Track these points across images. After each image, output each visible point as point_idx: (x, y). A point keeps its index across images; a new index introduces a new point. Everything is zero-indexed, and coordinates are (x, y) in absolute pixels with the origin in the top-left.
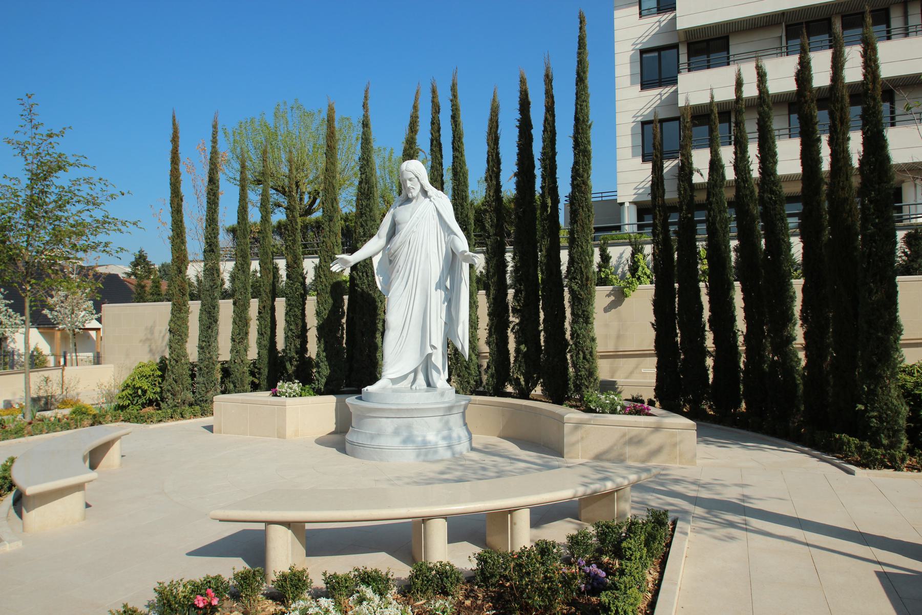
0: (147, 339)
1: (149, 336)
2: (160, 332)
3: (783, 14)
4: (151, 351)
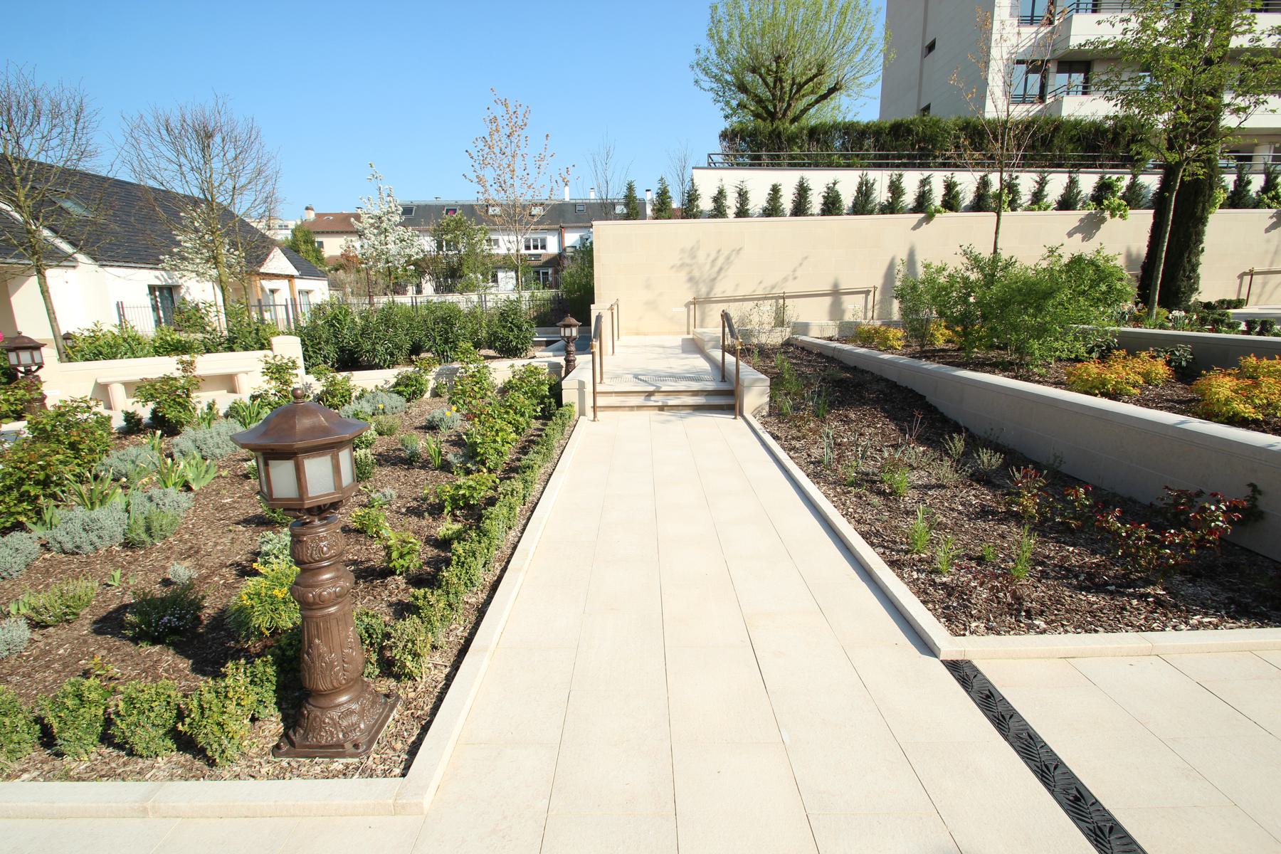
0: (682, 265)
1: (688, 261)
4: (691, 279)
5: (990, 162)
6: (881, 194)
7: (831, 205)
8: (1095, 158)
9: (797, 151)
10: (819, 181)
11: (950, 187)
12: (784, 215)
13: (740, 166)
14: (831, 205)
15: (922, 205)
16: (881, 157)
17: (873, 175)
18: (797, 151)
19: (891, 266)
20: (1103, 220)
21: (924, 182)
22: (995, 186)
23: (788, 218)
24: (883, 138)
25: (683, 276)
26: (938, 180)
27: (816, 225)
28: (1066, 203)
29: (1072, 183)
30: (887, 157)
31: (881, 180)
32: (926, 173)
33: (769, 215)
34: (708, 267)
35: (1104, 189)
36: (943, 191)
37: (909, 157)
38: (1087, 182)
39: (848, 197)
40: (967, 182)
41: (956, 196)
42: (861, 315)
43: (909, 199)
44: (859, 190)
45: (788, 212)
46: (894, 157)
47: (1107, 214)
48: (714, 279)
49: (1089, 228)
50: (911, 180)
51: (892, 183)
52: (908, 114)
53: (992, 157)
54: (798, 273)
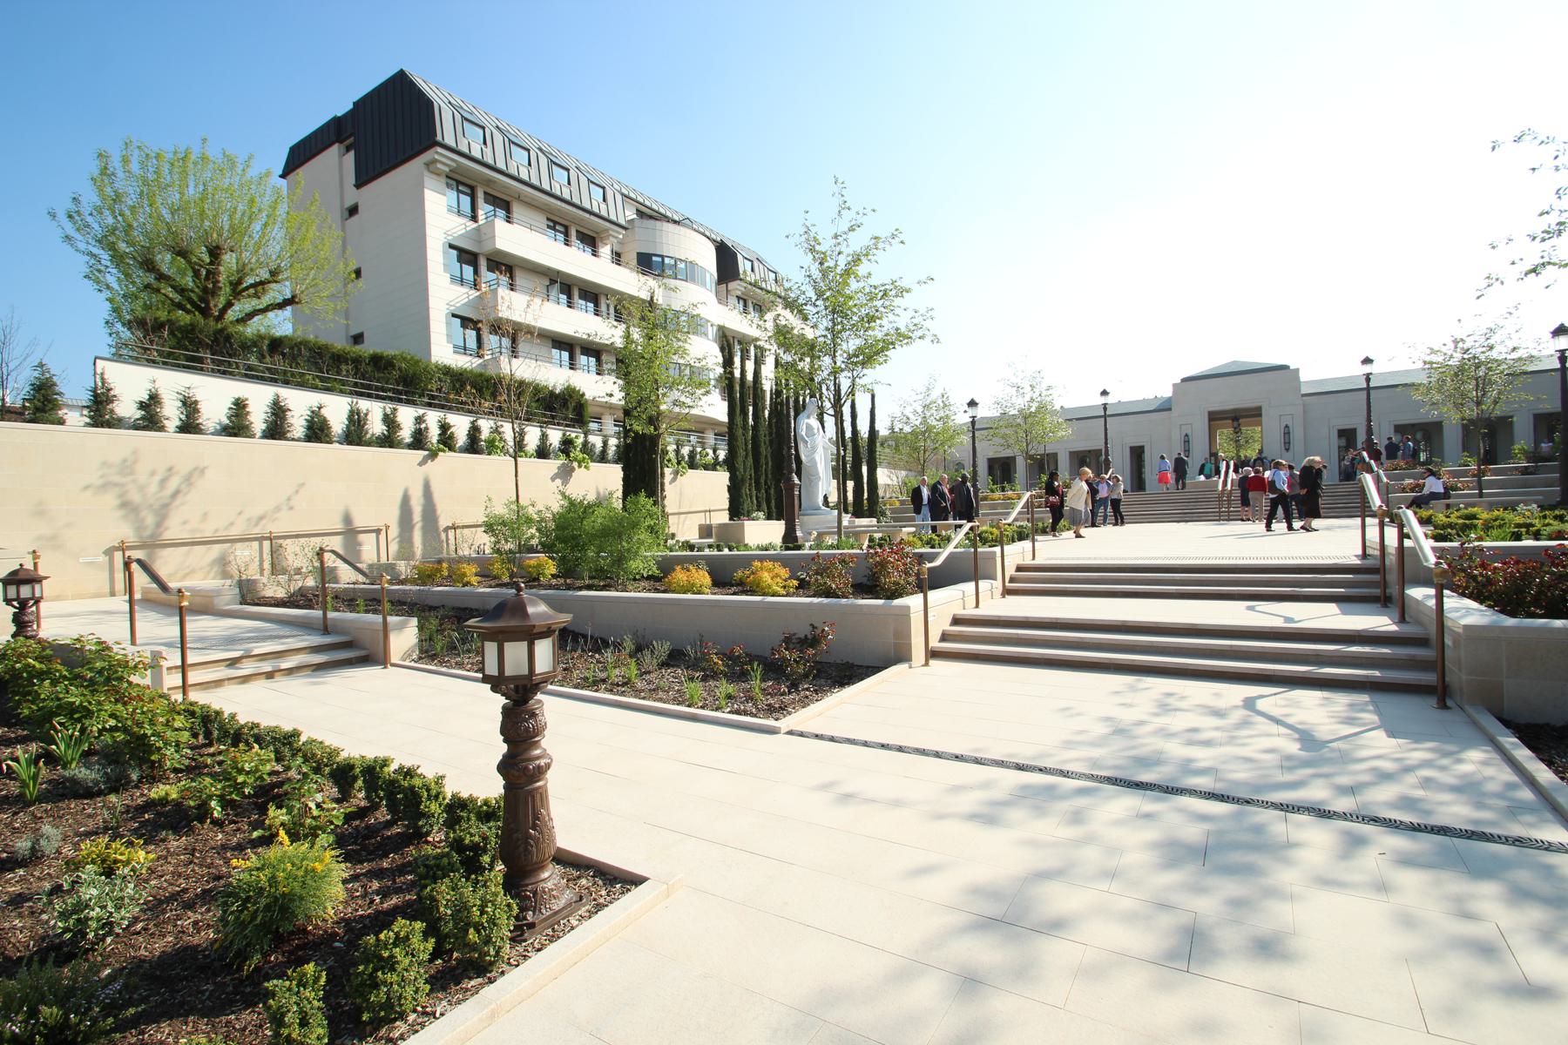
1: (117, 479)
3: (558, 272)
4: (125, 505)
5: (499, 412)
6: (376, 427)
7: (317, 431)
8: (553, 417)
9: (253, 361)
10: (300, 403)
11: (444, 427)
12: (253, 436)
13: (152, 363)
14: (236, 426)
15: (419, 441)
16: (363, 386)
17: (364, 404)
18: (253, 361)
19: (406, 500)
20: (573, 469)
21: (419, 420)
22: (485, 434)
23: (336, 445)
24: (363, 367)
25: (110, 499)
26: (433, 418)
27: (296, 453)
28: (542, 453)
29: (544, 437)
30: (369, 387)
31: (374, 412)
32: (421, 412)
33: (350, 443)
35: (567, 444)
36: (438, 432)
37: (394, 391)
38: (555, 436)
39: (338, 424)
40: (460, 424)
41: (451, 437)
42: (255, 566)
43: (406, 434)
44: (350, 418)
45: (259, 434)
46: (377, 389)
47: (575, 464)
48: (166, 506)
49: (565, 474)
50: (406, 416)
51: (386, 415)
52: (591, 410)
53: (500, 408)
54: (292, 503)
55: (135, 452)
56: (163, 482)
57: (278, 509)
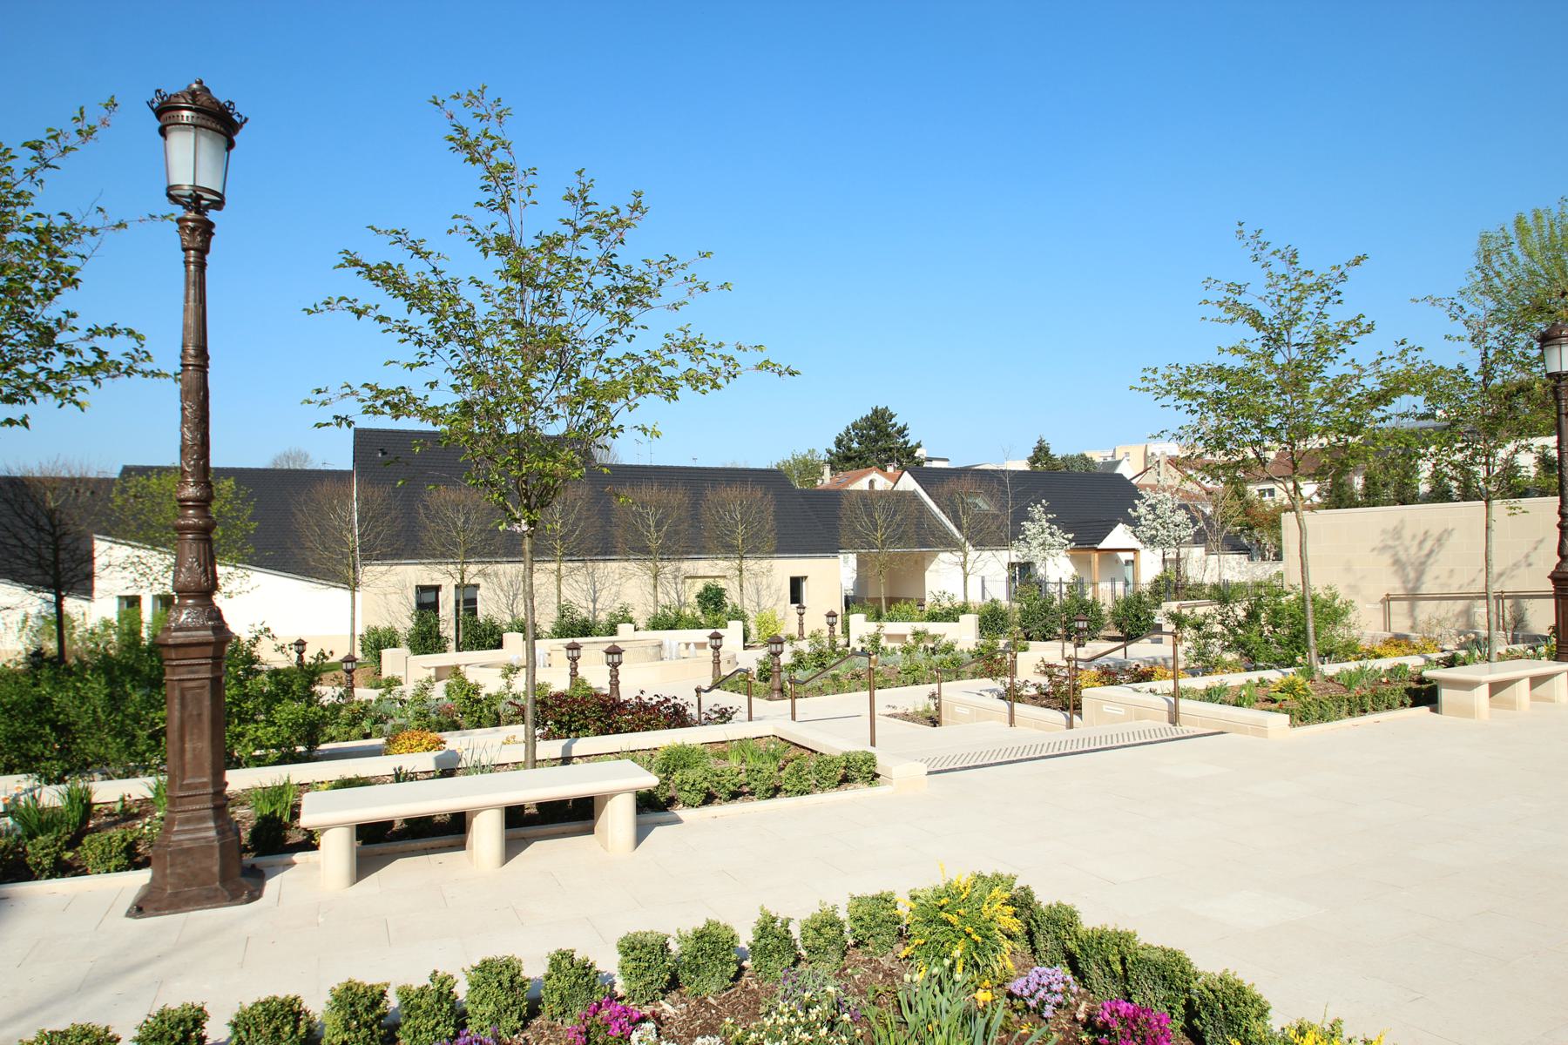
1: (1390, 543)
2: (1414, 537)
25: (1386, 559)
34: (1413, 550)
55: (1402, 521)
56: (1421, 543)
57: (1516, 565)
